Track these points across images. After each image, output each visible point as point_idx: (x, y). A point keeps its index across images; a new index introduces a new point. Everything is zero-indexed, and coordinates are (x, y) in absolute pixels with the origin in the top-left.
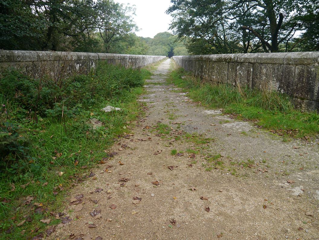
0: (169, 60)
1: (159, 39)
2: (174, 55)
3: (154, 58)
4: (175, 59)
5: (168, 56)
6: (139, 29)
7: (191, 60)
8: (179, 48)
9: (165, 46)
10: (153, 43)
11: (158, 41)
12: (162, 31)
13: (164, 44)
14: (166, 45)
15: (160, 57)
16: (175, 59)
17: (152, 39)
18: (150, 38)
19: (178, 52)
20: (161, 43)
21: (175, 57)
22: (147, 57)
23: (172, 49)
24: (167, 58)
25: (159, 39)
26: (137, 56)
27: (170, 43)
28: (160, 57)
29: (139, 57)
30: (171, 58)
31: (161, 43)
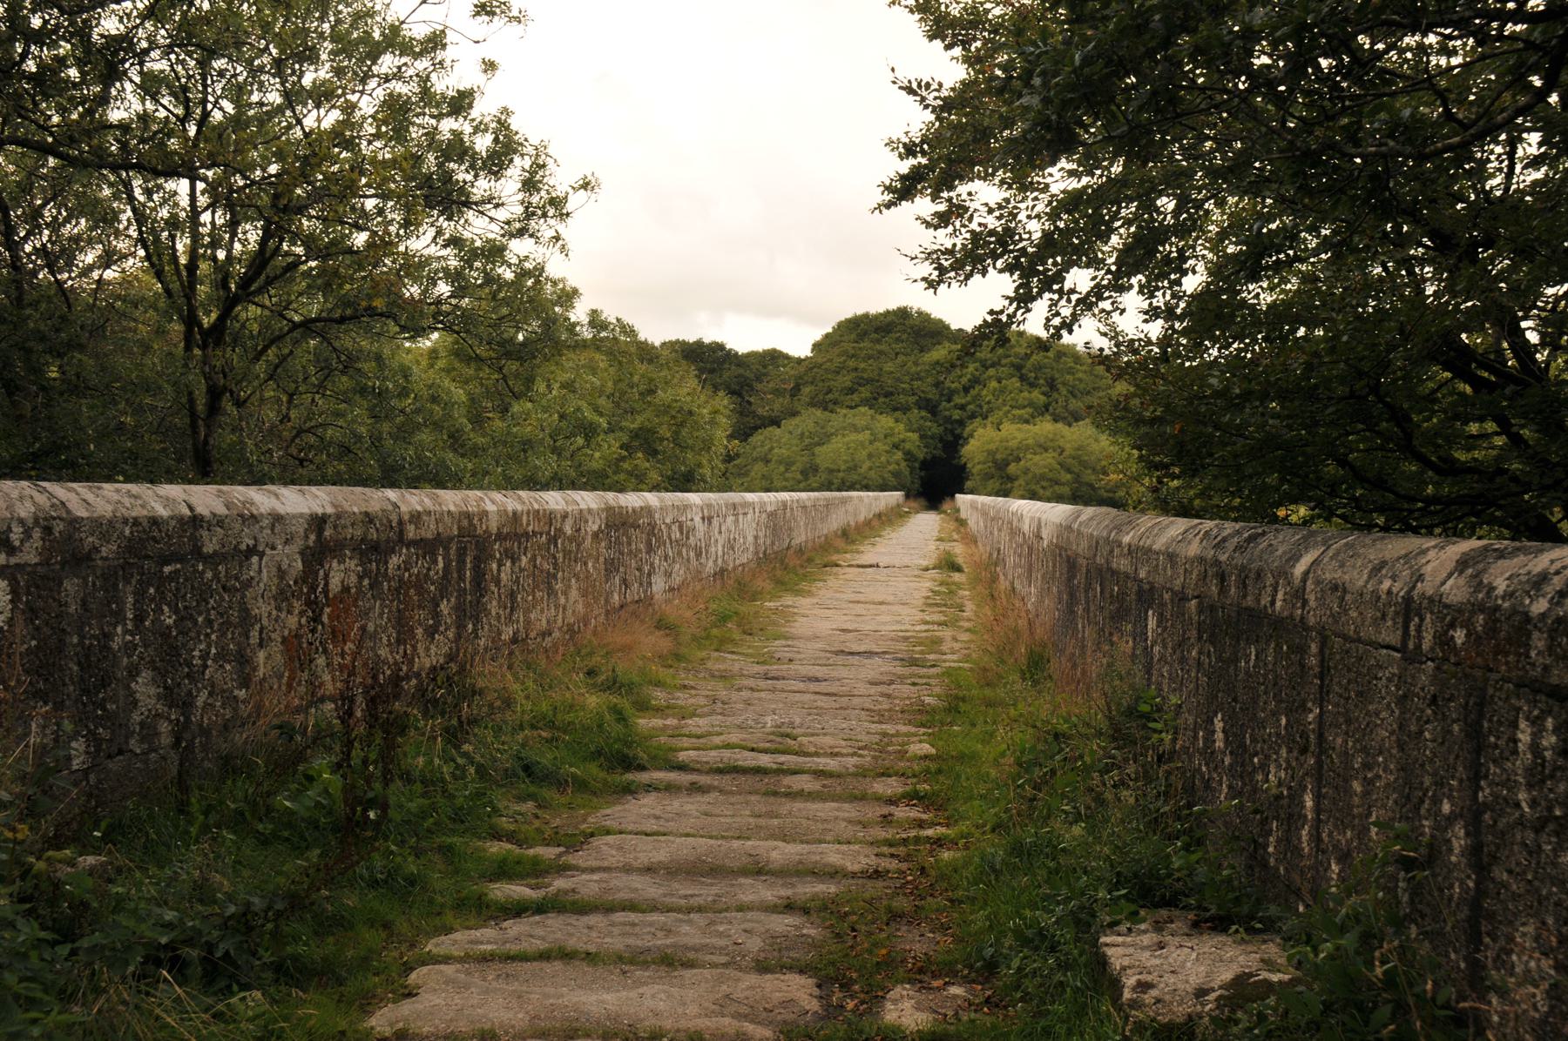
0: (925, 526)
1: (851, 363)
2: (969, 484)
3: (776, 521)
4: (975, 523)
5: (919, 495)
6: (559, 179)
7: (1279, 625)
8: (1008, 428)
9: (898, 414)
10: (806, 390)
11: (845, 380)
12: (878, 302)
13: (883, 397)
14: (905, 409)
15: (844, 501)
16: (971, 523)
17: (799, 361)
18: (787, 357)
19: (1001, 466)
20: (865, 392)
21: (973, 506)
22: (686, 507)
23: (952, 441)
24: (914, 504)
25: (851, 363)
26: (495, 503)
27: (932, 394)
28: (844, 501)
29: (550, 517)
30: (946, 506)
31: (865, 392)
